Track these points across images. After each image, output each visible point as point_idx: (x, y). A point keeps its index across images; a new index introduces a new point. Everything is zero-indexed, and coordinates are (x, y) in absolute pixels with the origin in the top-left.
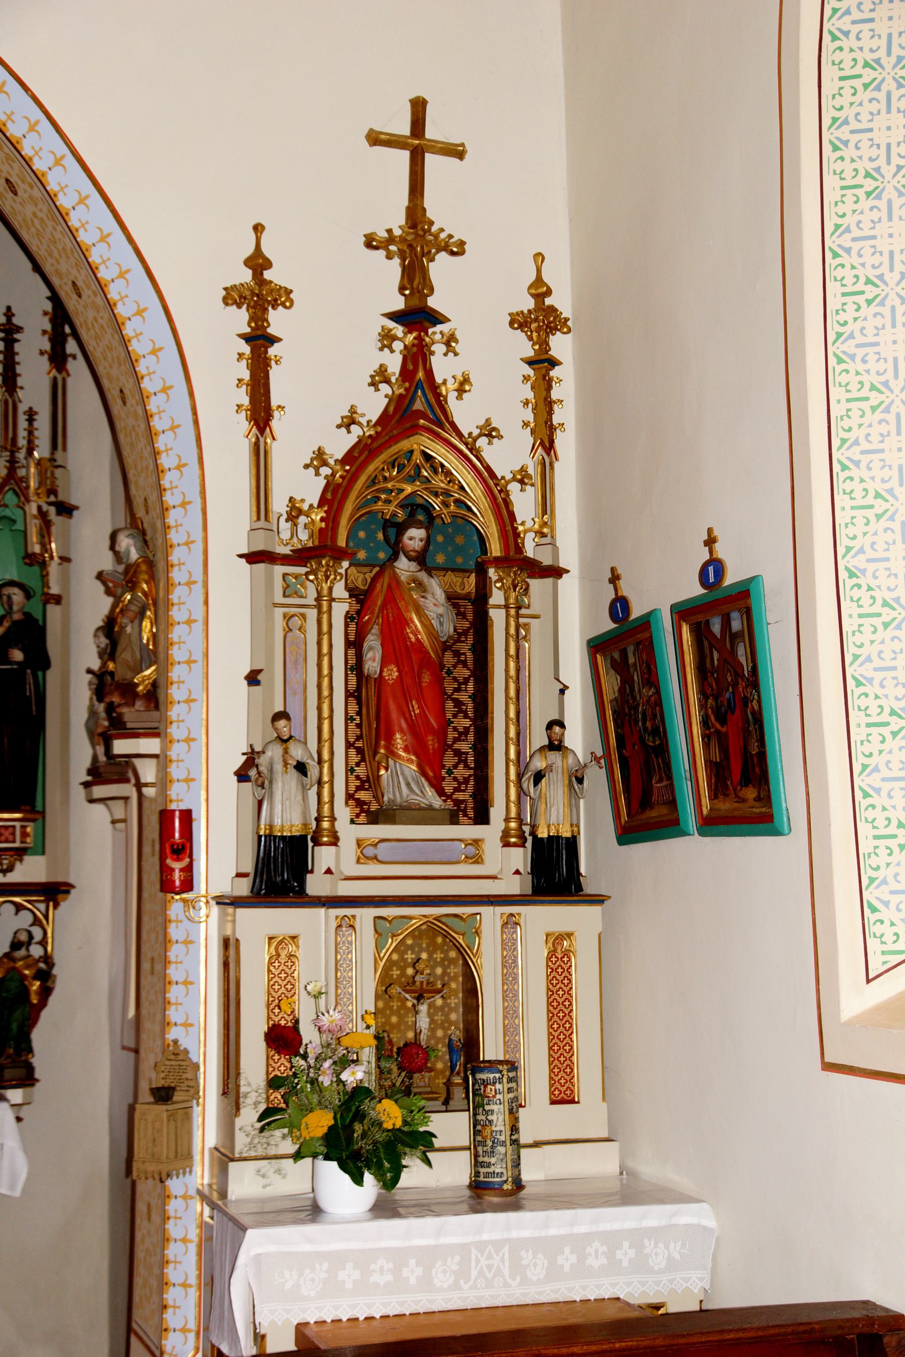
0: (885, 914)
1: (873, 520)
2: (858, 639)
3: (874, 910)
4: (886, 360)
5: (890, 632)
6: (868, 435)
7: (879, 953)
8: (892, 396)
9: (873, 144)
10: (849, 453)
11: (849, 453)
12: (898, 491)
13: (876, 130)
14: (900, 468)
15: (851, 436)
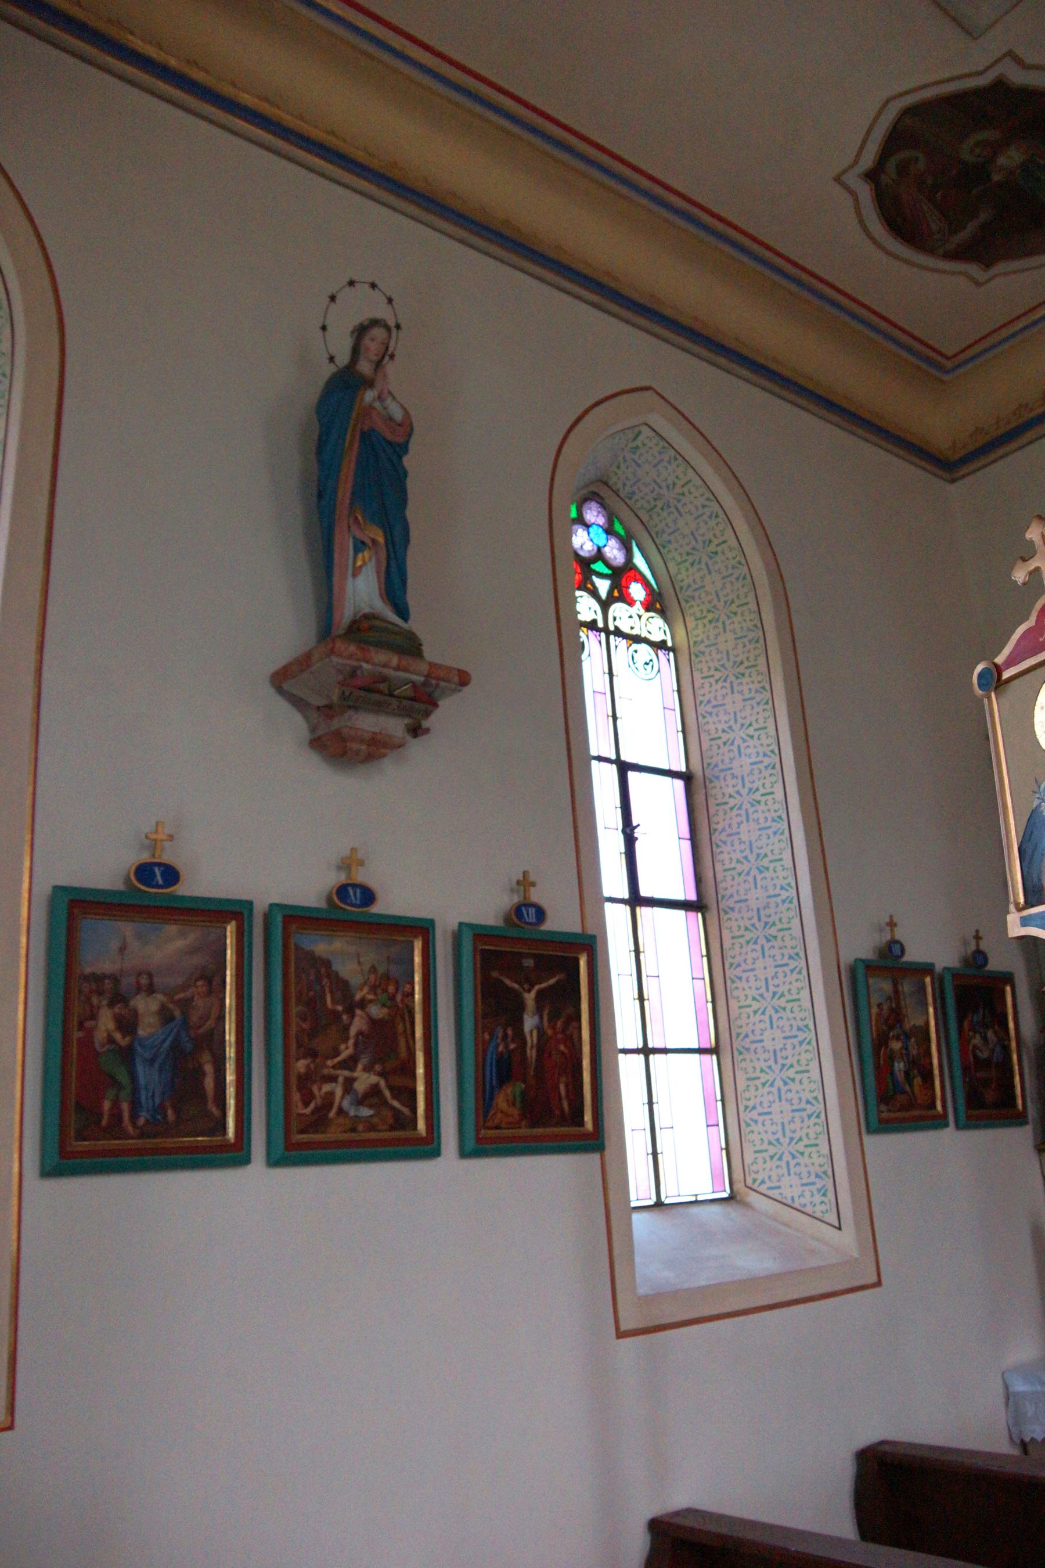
0: (716, 783)
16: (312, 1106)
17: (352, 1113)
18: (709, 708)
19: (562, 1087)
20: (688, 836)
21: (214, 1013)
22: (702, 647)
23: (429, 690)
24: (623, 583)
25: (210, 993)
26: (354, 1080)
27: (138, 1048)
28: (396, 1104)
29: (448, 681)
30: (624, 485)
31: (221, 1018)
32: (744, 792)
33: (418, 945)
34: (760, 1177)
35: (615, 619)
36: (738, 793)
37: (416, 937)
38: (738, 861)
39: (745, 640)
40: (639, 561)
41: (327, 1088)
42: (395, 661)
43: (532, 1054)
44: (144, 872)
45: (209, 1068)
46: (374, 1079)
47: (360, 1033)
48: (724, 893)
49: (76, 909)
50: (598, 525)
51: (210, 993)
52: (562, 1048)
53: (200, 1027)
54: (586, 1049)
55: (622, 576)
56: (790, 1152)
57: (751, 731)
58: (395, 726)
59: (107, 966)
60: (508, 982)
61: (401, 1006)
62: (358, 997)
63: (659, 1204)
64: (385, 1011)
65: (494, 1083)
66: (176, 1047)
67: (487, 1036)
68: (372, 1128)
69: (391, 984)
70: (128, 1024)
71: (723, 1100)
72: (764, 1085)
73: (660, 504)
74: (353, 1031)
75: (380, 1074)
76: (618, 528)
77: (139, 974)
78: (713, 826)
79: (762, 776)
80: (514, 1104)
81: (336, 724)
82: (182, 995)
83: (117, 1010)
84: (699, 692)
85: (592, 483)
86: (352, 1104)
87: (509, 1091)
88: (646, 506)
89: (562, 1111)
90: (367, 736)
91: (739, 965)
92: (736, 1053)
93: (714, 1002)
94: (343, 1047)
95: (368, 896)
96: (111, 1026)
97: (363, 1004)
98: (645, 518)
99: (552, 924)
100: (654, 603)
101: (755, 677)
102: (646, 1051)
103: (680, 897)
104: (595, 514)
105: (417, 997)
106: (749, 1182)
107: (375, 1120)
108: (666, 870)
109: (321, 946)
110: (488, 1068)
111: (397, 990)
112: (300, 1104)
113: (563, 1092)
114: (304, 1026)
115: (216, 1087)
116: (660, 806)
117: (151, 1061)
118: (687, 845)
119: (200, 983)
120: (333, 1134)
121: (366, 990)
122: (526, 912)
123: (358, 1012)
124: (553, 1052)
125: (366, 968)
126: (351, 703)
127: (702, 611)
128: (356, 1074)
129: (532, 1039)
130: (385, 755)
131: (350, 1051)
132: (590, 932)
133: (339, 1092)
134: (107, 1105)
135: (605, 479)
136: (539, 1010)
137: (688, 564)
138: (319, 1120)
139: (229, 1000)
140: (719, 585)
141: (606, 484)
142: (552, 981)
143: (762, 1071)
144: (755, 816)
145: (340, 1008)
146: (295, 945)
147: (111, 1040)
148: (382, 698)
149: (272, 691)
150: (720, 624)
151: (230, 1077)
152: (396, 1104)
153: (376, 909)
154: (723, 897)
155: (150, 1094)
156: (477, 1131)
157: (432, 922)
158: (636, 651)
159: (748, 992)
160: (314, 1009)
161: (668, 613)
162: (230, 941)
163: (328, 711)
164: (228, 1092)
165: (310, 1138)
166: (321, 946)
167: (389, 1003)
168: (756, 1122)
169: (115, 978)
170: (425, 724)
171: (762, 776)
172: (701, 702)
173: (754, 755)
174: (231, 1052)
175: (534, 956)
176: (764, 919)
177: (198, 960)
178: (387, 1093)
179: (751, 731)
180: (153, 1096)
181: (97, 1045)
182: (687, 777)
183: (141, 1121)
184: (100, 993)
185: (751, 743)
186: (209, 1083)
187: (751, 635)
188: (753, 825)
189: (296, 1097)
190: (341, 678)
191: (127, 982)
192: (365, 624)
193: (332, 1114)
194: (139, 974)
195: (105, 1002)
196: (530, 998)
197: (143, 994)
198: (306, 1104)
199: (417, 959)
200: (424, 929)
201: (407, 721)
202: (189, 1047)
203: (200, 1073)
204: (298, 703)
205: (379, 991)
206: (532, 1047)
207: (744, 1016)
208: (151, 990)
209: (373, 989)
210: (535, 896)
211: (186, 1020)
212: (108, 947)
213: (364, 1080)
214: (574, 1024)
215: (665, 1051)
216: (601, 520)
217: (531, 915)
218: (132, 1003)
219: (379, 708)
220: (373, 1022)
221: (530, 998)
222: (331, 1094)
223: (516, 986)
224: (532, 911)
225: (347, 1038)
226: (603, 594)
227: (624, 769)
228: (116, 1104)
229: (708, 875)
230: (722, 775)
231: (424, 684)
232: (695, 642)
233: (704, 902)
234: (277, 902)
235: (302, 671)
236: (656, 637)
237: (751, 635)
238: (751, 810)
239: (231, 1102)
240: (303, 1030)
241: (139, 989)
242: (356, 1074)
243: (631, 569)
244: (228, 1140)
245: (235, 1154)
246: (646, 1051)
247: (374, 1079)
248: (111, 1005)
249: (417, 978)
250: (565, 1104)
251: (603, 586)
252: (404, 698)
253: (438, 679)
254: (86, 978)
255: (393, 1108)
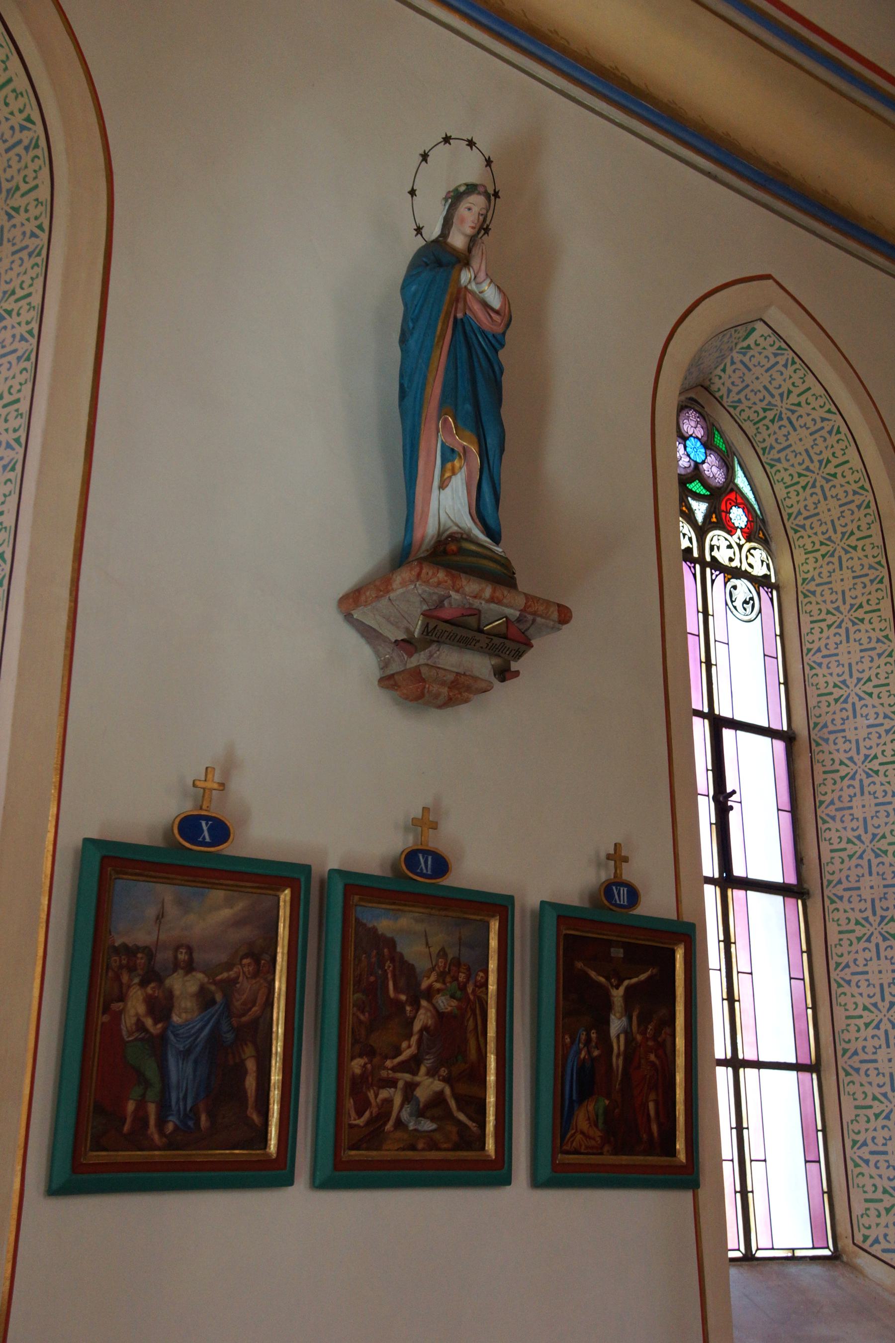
0: (824, 747)
1: (846, 859)
2: (839, 950)
3: (818, 744)
4: (836, 593)
5: (881, 1122)
6: (821, 573)
7: (821, 773)
8: (872, 929)
9: (876, 815)
10: (842, 974)
11: (842, 974)
12: (890, 1094)
13: (834, 582)
14: (891, 1075)
15: (844, 961)
16: (367, 1114)
17: (411, 1126)
18: (818, 658)
19: (651, 1106)
20: (788, 808)
21: (261, 1000)
22: (812, 586)
23: (523, 627)
24: (723, 507)
25: (255, 975)
26: (417, 1085)
27: (172, 1037)
28: (462, 1117)
29: (547, 618)
30: (729, 391)
31: (269, 1004)
32: (859, 759)
33: (494, 926)
34: (873, 1234)
35: (712, 548)
36: (851, 759)
37: (493, 916)
38: (849, 841)
39: (866, 580)
40: (741, 480)
41: (384, 1094)
42: (488, 592)
43: (618, 1063)
44: (189, 826)
45: (251, 1065)
46: (437, 1085)
47: (425, 1028)
48: (831, 878)
49: (110, 866)
50: (697, 438)
51: (255, 975)
52: (652, 1057)
53: (244, 1015)
54: (680, 1061)
55: (721, 497)
56: (855, 763)
57: (869, 687)
58: (480, 665)
59: (142, 937)
60: (593, 974)
61: (472, 997)
62: (425, 984)
63: (749, 1257)
64: (454, 1003)
65: (574, 1097)
66: (215, 1038)
67: (568, 1040)
68: (433, 1146)
69: (463, 971)
70: (161, 1008)
71: (824, 1130)
72: (877, 1116)
73: (770, 415)
74: (417, 1026)
75: (447, 1080)
76: (718, 441)
77: (177, 948)
78: (820, 798)
79: (882, 741)
80: (596, 1125)
81: (415, 661)
82: (225, 975)
83: (149, 990)
84: (807, 638)
85: (692, 388)
86: (411, 1115)
87: (590, 1108)
88: (754, 416)
89: (650, 1133)
90: (450, 677)
91: (847, 966)
92: (842, 1074)
93: (814, 1008)
94: (404, 1045)
95: (441, 866)
96: (141, 1009)
97: (429, 994)
98: (751, 431)
99: (645, 909)
100: (757, 532)
101: (876, 625)
102: (736, 1063)
103: (777, 878)
104: (693, 424)
105: (492, 987)
106: (859, 1238)
107: (438, 1136)
108: (761, 847)
109: (386, 922)
110: (568, 1078)
111: (468, 978)
112: (353, 1114)
113: (652, 1113)
114: (362, 1017)
115: (258, 1089)
116: (755, 768)
117: (185, 1054)
118: (786, 817)
119: (245, 961)
120: (388, 1153)
121: (433, 977)
122: (617, 892)
123: (424, 1003)
124: (643, 1061)
125: (435, 950)
126: (433, 638)
127: (813, 543)
128: (417, 1079)
129: (618, 1045)
130: (466, 701)
131: (413, 1050)
132: (686, 918)
133: (398, 1100)
134: (131, 1106)
135: (707, 383)
136: (628, 1011)
137: (798, 487)
138: (373, 1135)
139: (280, 984)
140: (836, 513)
141: (707, 389)
142: (643, 977)
143: (875, 1098)
144: (872, 788)
145: (403, 997)
146: (356, 919)
147: (140, 1026)
148: (470, 634)
149: (339, 618)
150: (835, 560)
151: (276, 1077)
152: (462, 1117)
153: (449, 881)
154: (830, 882)
155: (181, 1095)
156: (554, 1157)
157: (511, 899)
158: (735, 587)
159: (858, 999)
160: (375, 994)
161: (773, 546)
162: (284, 912)
163: (408, 645)
164: (271, 1094)
165: (362, 1158)
166: (386, 922)
167: (459, 994)
168: (867, 1162)
169: (149, 952)
170: (514, 666)
171: (882, 741)
172: (809, 650)
173: (872, 716)
174: (278, 1047)
175: (626, 946)
176: (879, 912)
177: (246, 933)
178: (453, 1104)
179: (869, 687)
180: (185, 1098)
181: (124, 1033)
182: (788, 738)
183: (170, 1127)
184: (132, 969)
185: (868, 701)
186: (250, 1083)
187: (873, 574)
188: (868, 800)
189: (350, 1103)
190: (425, 607)
191: (163, 957)
192: (453, 547)
193: (389, 1126)
194: (177, 948)
195: (136, 980)
196: (617, 995)
197: (181, 972)
198: (360, 1114)
199: (493, 943)
200: (500, 906)
201: (495, 661)
202: (229, 1037)
203: (242, 1072)
204: (368, 633)
205: (448, 979)
206: (618, 1056)
207: (853, 1028)
208: (190, 967)
209: (442, 977)
210: (629, 874)
211: (228, 1005)
212: (151, 915)
213: (428, 1086)
214: (668, 1030)
215: (758, 1065)
216: (699, 432)
217: (622, 896)
218: (168, 982)
219: (465, 643)
220: (440, 1016)
221: (617, 995)
222: (389, 1102)
223: (602, 979)
224: (624, 891)
225: (411, 1035)
226: (700, 517)
227: (718, 724)
228: (141, 1105)
229: (811, 854)
230: (832, 737)
231: (519, 620)
232: (804, 580)
233: (805, 886)
234: (336, 867)
235: (378, 598)
236: (759, 571)
237: (873, 574)
238: (866, 782)
239: (275, 1108)
240: (361, 1022)
241: (176, 966)
242: (417, 1079)
243: (732, 490)
244: (269, 1155)
245: (275, 1173)
246: (736, 1063)
247: (437, 1085)
248: (143, 984)
249: (493, 965)
250: (654, 1128)
251: (700, 509)
252: (495, 635)
253: (535, 614)
254: (116, 950)
255: (459, 1122)
